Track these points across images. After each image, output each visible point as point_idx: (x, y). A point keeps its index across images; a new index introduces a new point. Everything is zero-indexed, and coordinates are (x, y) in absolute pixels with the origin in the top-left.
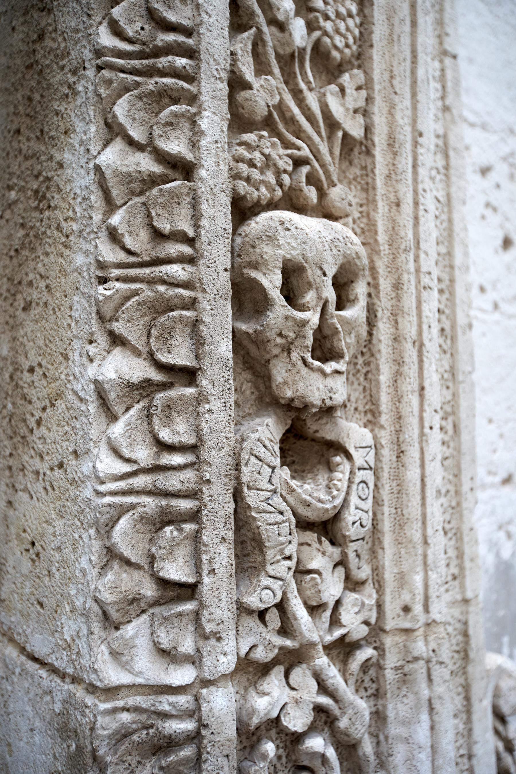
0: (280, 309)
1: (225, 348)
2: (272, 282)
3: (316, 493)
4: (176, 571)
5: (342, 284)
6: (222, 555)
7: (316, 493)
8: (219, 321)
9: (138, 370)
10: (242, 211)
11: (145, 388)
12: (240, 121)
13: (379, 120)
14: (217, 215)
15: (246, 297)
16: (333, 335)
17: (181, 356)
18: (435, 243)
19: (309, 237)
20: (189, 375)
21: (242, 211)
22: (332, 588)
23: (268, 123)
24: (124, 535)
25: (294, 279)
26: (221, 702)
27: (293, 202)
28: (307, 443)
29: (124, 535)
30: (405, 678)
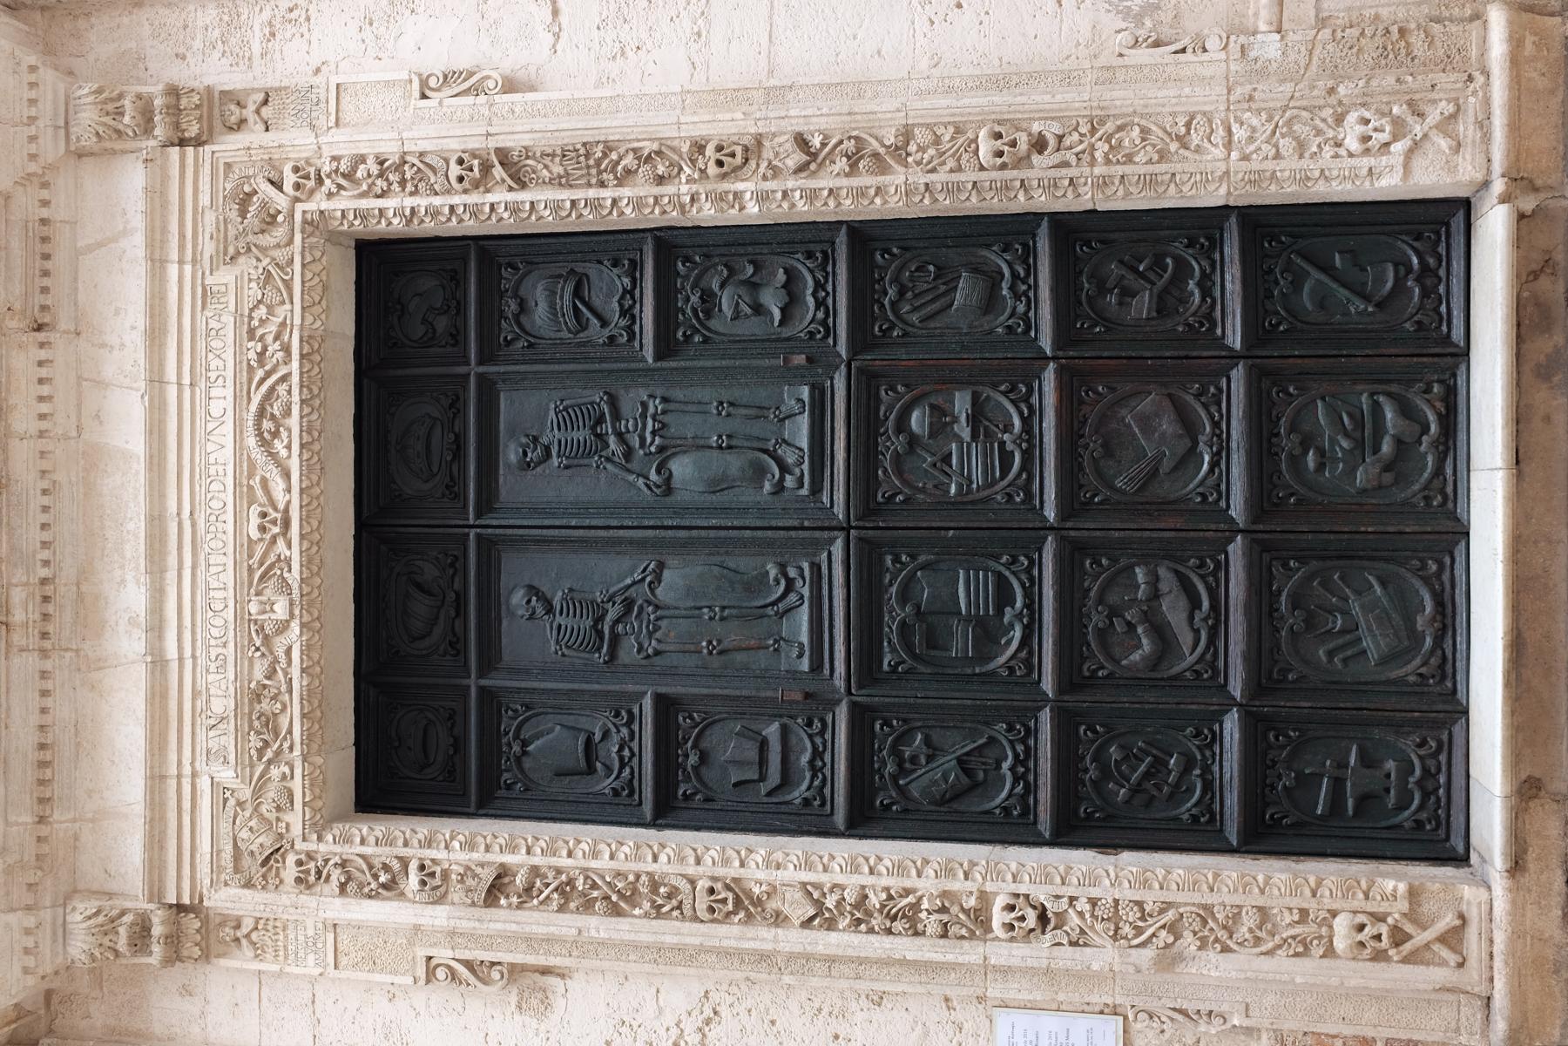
0: (1005, 159)
1: (1015, 172)
2: (999, 161)
3: (1052, 142)
4: (1066, 182)
5: (999, 136)
6: (1064, 171)
7: (1052, 142)
8: (1009, 174)
9: (1021, 193)
10: (982, 168)
11: (1026, 190)
12: (959, 169)
13: (946, 120)
14: (984, 175)
15: (1003, 166)
16: (333, 237)
17: (1018, 184)
18: (246, 892)
19: (985, 148)
20: (1022, 181)
21: (982, 168)
22: (1076, 136)
23: (959, 160)
24: (1059, 194)
25: (1000, 154)
26: (1097, 171)
27: (976, 151)
28: (1039, 145)
29: (1059, 194)
30: (1102, 109)
